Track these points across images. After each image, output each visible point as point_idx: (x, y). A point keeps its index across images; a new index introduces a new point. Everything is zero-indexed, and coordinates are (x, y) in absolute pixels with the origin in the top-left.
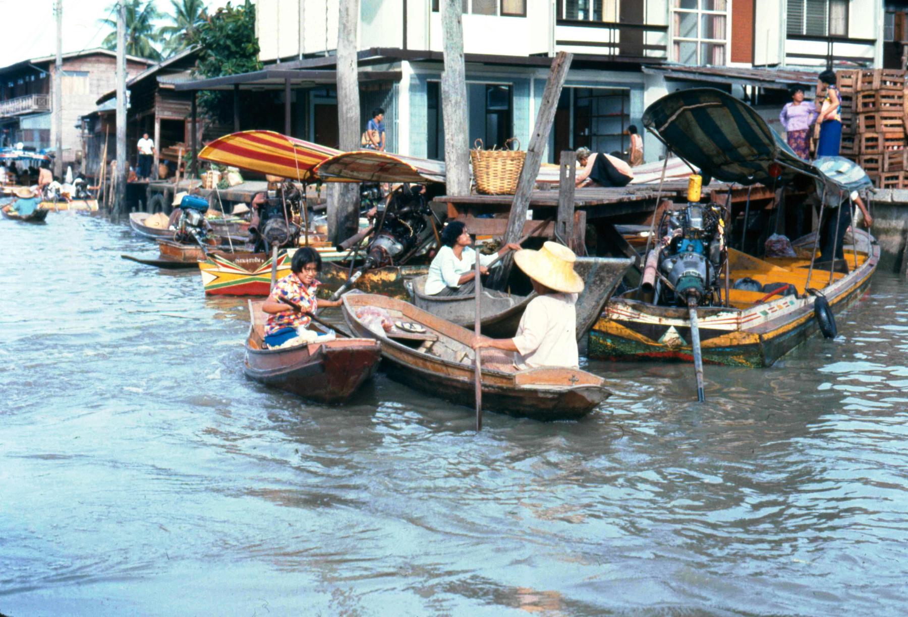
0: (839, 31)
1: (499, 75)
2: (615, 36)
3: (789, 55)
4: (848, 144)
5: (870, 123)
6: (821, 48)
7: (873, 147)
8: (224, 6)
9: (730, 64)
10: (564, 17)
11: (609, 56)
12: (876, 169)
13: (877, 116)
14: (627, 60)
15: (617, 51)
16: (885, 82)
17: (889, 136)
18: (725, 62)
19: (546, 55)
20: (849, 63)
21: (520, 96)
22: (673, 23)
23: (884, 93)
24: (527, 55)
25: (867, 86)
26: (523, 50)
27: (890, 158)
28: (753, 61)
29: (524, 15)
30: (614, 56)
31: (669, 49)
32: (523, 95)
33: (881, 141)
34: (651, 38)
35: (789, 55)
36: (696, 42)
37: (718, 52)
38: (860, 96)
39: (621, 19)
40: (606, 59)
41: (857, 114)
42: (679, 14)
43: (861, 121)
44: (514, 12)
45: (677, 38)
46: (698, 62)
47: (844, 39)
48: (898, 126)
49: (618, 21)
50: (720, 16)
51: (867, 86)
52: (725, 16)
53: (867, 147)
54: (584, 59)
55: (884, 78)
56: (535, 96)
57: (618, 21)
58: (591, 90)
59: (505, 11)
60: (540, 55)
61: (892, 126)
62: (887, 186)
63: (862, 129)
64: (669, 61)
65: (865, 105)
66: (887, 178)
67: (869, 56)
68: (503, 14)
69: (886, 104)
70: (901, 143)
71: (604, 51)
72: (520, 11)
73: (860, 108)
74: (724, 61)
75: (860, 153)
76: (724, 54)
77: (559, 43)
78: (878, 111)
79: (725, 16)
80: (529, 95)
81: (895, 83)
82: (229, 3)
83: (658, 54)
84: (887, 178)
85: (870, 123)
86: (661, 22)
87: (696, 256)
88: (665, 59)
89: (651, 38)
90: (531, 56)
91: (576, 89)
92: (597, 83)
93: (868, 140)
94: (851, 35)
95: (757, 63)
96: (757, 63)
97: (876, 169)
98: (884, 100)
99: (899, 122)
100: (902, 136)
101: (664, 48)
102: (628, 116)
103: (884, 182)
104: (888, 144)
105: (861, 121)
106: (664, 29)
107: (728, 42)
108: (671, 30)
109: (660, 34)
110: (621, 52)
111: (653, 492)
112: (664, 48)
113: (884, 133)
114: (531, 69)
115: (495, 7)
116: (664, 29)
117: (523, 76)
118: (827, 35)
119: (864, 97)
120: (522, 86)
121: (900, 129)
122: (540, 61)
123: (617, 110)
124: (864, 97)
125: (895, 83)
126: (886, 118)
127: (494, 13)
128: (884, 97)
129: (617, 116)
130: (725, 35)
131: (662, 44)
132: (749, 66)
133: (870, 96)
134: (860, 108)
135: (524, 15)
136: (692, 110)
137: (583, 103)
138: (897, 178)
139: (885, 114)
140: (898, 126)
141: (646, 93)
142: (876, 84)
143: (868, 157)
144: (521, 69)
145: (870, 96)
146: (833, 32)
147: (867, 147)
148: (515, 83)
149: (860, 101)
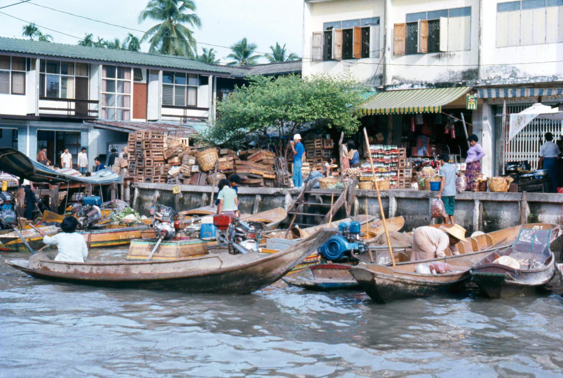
0: (192, 102)
1: (11, 124)
2: (73, 105)
3: (163, 115)
4: (140, 163)
5: (148, 154)
6: (180, 112)
7: (150, 164)
8: (198, 13)
9: (133, 120)
10: (46, 96)
11: (68, 115)
12: (150, 174)
13: (151, 151)
14: (77, 118)
15: (73, 113)
16: (154, 136)
17: (156, 160)
18: (131, 119)
19: (34, 114)
20: (196, 119)
21: (21, 134)
22: (102, 100)
23: (153, 141)
24: (25, 115)
25: (146, 138)
26: (23, 112)
27: (156, 169)
28: (146, 118)
29: (24, 94)
30: (70, 116)
31: (99, 112)
32: (23, 134)
33: (152, 161)
34: (92, 107)
35: (163, 115)
36: (115, 109)
37: (126, 114)
38: (144, 142)
39: (76, 97)
40: (66, 117)
41: (143, 150)
42: (106, 94)
43: (145, 153)
44: (19, 92)
45: (104, 107)
46: (118, 119)
47: (195, 108)
48: (161, 155)
49: (74, 98)
50: (127, 96)
51: (146, 138)
52: (130, 96)
53: (147, 164)
54: (52, 116)
55: (153, 135)
56: (30, 134)
57: (74, 98)
58: (64, 132)
59: (14, 92)
60: (31, 114)
61: (158, 155)
62: (155, 182)
63: (145, 156)
64: (100, 118)
65: (146, 146)
66: (155, 178)
67: (206, 116)
68: (12, 93)
69: (154, 146)
70: (162, 163)
71: (65, 113)
72: (22, 92)
73: (144, 148)
74: (130, 118)
75: (144, 167)
76: (130, 114)
77: (41, 108)
78: (151, 149)
79: (130, 96)
80: (26, 134)
81: (159, 137)
82: (91, 35)
83: (94, 114)
84: (155, 178)
85: (148, 154)
86: (96, 99)
87: (9, 211)
88: (98, 117)
89: (92, 107)
90: (28, 115)
91: (57, 132)
92: (63, 128)
93: (148, 161)
94: (198, 106)
95: (149, 118)
96: (149, 118)
97: (150, 174)
98: (153, 144)
99: (161, 153)
100: (163, 159)
101: (97, 112)
102: (80, 145)
103: (153, 180)
104: (155, 163)
105: (145, 153)
106: (97, 102)
107: (131, 108)
108: (100, 103)
109: (95, 105)
110: (76, 113)
111: (435, 315)
112: (97, 112)
113: (153, 158)
114: (27, 121)
115: (9, 90)
116: (97, 102)
117: (24, 125)
118: (186, 106)
119: (146, 142)
120: (23, 129)
121: (162, 157)
122: (31, 117)
123: (75, 143)
124: (146, 142)
125: (159, 137)
126: (155, 152)
127: (8, 93)
128: (154, 143)
129: (75, 145)
130: (130, 105)
131: (97, 109)
132: (144, 120)
133: (148, 142)
134: (144, 148)
135: (24, 94)
136: (7, 155)
137: (61, 138)
138: (158, 178)
139: (154, 150)
140: (161, 155)
141: (89, 134)
142: (150, 137)
143: (148, 169)
144: (22, 121)
145: (148, 142)
146: (189, 104)
147: (147, 164)
148: (19, 128)
149: (144, 144)
